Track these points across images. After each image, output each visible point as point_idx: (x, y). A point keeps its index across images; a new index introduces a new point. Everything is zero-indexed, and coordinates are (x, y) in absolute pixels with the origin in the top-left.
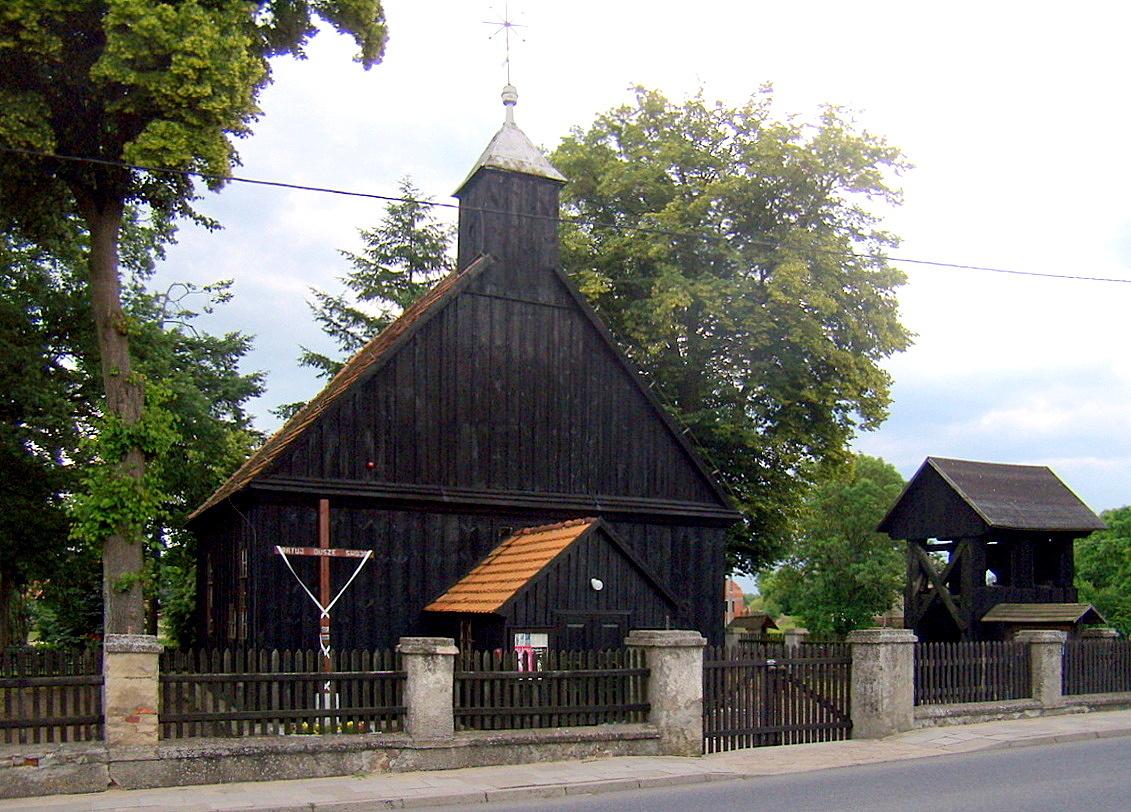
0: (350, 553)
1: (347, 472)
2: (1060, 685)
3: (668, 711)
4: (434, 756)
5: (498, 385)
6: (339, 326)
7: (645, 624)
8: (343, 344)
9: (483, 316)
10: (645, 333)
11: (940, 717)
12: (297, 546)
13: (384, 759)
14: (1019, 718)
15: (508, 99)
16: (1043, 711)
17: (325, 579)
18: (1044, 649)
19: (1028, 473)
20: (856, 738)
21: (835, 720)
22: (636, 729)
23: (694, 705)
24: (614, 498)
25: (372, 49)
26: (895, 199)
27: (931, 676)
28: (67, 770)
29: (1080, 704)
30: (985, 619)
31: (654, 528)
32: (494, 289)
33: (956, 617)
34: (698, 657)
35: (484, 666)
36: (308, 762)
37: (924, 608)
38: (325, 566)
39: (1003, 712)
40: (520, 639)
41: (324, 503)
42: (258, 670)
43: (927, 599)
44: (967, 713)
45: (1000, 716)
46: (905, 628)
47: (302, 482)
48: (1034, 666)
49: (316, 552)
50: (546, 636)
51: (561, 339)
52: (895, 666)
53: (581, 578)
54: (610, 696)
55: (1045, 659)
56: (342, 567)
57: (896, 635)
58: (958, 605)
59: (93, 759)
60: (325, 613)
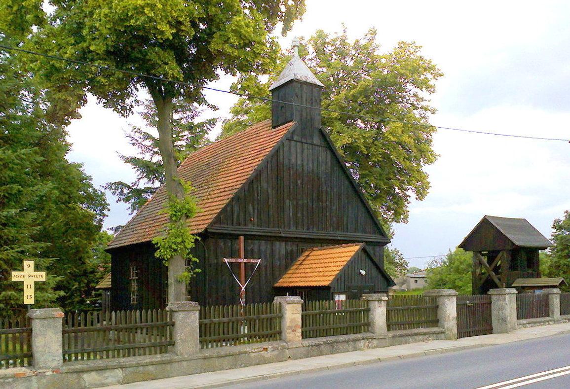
0: (252, 261)
4: (383, 343)
6: (137, 141)
8: (140, 150)
12: (232, 258)
13: (367, 343)
18: (554, 296)
22: (435, 329)
24: (343, 233)
26: (431, 89)
28: (276, 353)
32: (297, 137)
35: (143, 320)
36: (217, 362)
37: (482, 282)
38: (243, 266)
40: (337, 298)
42: (359, 307)
43: (484, 277)
45: (542, 324)
46: (191, 301)
48: (550, 303)
50: (345, 296)
51: (322, 162)
53: (356, 270)
58: (500, 280)
59: (283, 348)
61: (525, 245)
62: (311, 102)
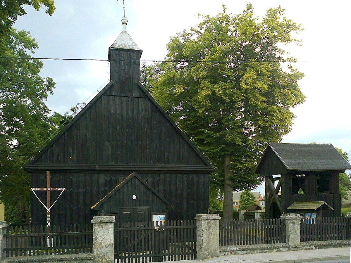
0: (57, 189)
1: (62, 161)
2: (299, 237)
3: (98, 249)
5: (118, 127)
7: (111, 212)
9: (112, 103)
10: (198, 106)
11: (233, 251)
14: (276, 251)
15: (124, 22)
16: (289, 249)
17: (48, 198)
19: (309, 146)
20: (205, 258)
21: (188, 251)
23: (110, 246)
25: (50, 12)
27: (329, 229)
29: (310, 246)
30: (288, 208)
31: (180, 175)
32: (116, 93)
33: (279, 207)
34: (111, 227)
38: (48, 194)
39: (267, 249)
41: (48, 172)
44: (248, 249)
45: (266, 251)
47: (41, 166)
49: (45, 189)
51: (142, 109)
52: (209, 229)
54: (276, 235)
55: (291, 226)
56: (54, 194)
57: (210, 217)
60: (48, 210)
61: (316, 169)
62: (129, 64)
